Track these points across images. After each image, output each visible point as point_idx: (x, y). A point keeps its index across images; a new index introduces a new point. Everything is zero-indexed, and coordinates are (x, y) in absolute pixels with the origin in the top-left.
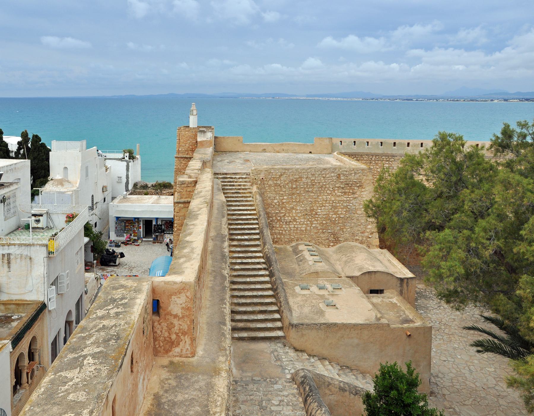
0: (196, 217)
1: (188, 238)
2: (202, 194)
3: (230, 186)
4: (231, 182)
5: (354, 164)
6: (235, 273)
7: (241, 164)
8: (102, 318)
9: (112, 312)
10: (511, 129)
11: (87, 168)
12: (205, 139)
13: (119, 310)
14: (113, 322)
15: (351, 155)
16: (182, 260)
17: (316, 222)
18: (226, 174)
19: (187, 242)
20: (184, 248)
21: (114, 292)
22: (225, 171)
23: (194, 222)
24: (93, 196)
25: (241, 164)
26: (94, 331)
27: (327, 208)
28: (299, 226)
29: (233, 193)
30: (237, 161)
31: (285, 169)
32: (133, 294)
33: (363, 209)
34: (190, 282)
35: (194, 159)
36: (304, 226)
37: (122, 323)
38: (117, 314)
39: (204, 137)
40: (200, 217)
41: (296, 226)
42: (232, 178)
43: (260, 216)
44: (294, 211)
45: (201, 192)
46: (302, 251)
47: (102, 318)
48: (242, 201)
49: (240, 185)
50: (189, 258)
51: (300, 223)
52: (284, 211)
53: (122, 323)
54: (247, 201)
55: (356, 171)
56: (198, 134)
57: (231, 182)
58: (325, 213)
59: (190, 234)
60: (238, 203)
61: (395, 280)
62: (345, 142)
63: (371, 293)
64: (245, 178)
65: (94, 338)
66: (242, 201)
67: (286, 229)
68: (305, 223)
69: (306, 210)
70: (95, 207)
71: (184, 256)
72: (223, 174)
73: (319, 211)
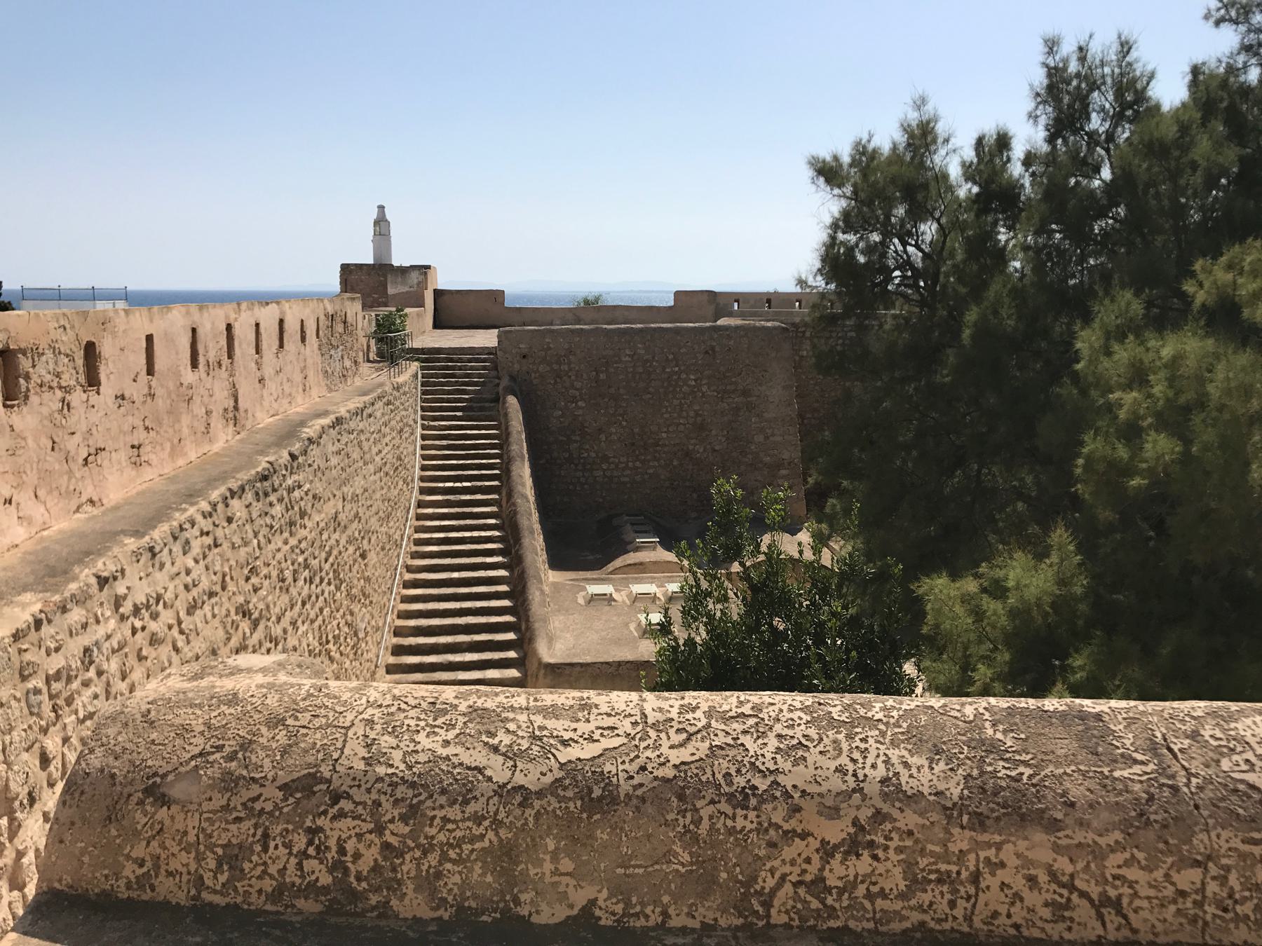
4: (447, 368)
10: (901, 139)
12: (406, 289)
17: (656, 463)
27: (681, 428)
28: (615, 474)
29: (449, 392)
33: (1047, 561)
36: (628, 472)
39: (404, 283)
41: (608, 473)
44: (603, 437)
49: (468, 376)
51: (617, 466)
52: (578, 438)
57: (447, 368)
58: (677, 441)
63: (98, 384)
67: (583, 480)
68: (630, 464)
73: (664, 435)
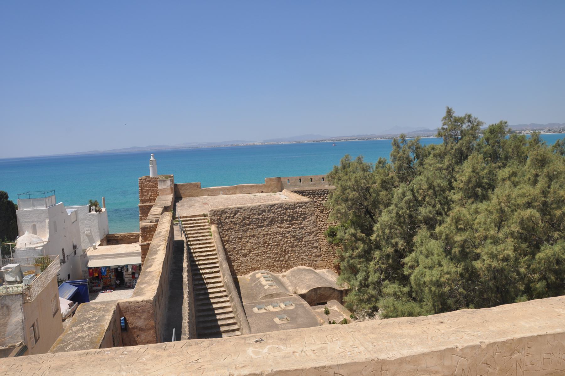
0: (156, 252)
1: (149, 270)
2: (162, 234)
3: (190, 227)
5: (305, 199)
6: (200, 303)
7: (200, 207)
8: (78, 331)
9: (85, 327)
11: (55, 223)
12: (166, 187)
13: (91, 325)
14: (87, 333)
15: (299, 192)
16: (143, 286)
18: (186, 217)
19: (149, 272)
20: (146, 276)
21: (86, 314)
22: (185, 215)
23: (154, 257)
24: (63, 250)
25: (200, 207)
26: (71, 340)
30: (197, 205)
31: (239, 208)
32: (102, 313)
34: (150, 300)
35: (156, 206)
37: (94, 333)
38: (90, 328)
40: (159, 252)
42: (192, 220)
43: (219, 251)
45: (161, 232)
46: (259, 278)
47: (78, 331)
48: (202, 240)
50: (148, 283)
53: (94, 333)
54: (206, 239)
55: (300, 205)
56: (159, 183)
59: (150, 266)
60: (198, 242)
61: (336, 293)
62: (292, 180)
64: (204, 219)
65: (71, 346)
66: (202, 240)
69: (259, 243)
70: (66, 259)
71: (146, 283)
72: (183, 217)
